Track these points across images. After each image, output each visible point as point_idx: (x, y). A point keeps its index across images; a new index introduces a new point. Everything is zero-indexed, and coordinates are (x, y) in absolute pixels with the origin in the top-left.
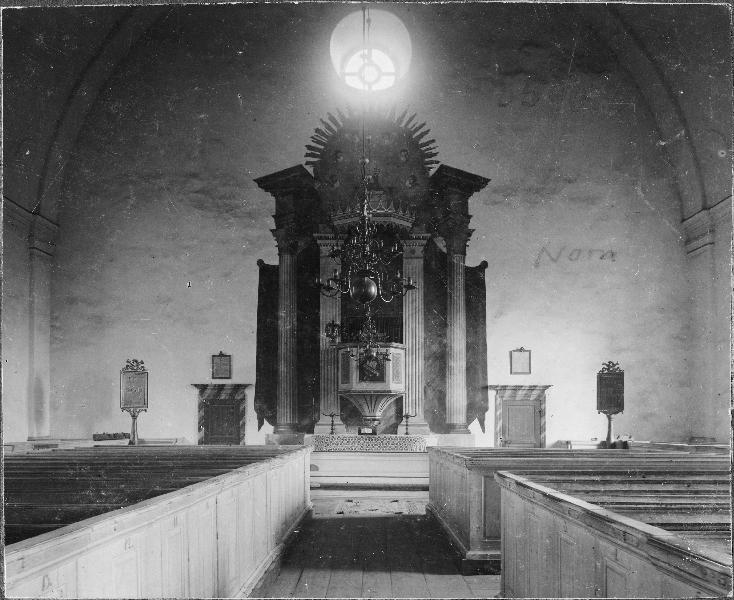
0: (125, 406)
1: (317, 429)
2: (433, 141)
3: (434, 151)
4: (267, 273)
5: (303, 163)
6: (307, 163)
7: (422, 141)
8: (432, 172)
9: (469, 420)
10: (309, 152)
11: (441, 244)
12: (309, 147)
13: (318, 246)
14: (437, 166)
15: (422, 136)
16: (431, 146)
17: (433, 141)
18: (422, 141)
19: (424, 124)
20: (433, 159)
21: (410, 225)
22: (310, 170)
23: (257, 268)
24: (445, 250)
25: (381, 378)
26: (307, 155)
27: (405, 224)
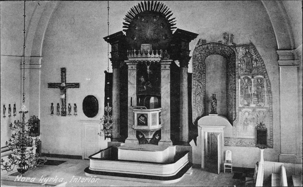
0: (40, 141)
1: (126, 141)
2: (174, 19)
3: (174, 23)
4: (108, 76)
5: (122, 30)
6: (124, 30)
7: (170, 19)
8: (173, 32)
9: (190, 140)
10: (124, 25)
11: (177, 63)
12: (124, 23)
13: (127, 66)
14: (176, 29)
15: (169, 17)
16: (173, 20)
17: (174, 19)
18: (170, 19)
19: (52, 104)
20: (174, 26)
21: (159, 59)
22: (125, 33)
23: (105, 74)
24: (179, 66)
25: (146, 124)
26: (123, 27)
27: (156, 59)
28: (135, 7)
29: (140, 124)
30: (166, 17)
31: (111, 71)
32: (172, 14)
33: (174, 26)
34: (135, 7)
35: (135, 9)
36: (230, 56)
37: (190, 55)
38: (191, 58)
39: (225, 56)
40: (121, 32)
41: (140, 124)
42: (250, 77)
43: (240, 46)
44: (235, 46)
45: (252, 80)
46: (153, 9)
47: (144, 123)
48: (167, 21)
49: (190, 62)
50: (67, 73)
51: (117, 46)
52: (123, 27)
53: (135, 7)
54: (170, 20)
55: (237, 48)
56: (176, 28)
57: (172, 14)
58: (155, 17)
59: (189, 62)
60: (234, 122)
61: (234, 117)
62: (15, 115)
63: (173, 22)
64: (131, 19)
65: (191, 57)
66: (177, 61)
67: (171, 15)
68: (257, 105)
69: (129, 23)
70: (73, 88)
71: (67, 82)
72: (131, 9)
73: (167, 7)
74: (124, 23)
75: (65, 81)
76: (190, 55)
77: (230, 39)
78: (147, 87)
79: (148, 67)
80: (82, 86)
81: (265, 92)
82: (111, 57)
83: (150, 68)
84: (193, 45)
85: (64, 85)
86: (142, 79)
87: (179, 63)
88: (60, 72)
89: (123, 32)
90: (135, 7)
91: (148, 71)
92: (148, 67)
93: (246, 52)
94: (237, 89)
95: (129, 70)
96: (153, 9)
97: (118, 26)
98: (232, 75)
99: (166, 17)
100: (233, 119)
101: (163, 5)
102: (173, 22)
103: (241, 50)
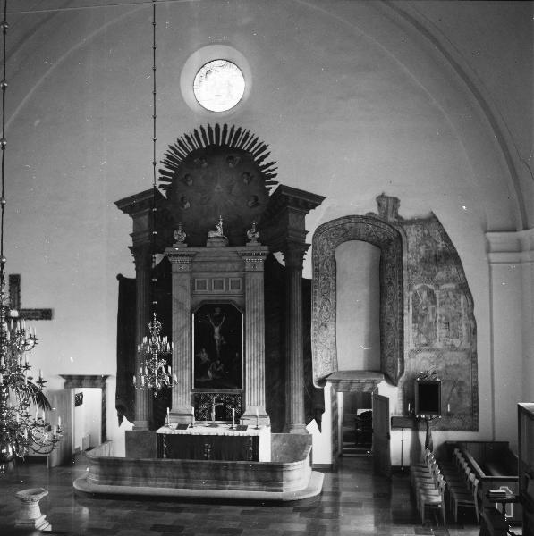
2: (272, 163)
3: (272, 173)
6: (161, 186)
7: (264, 163)
10: (162, 176)
11: (280, 257)
12: (162, 172)
14: (276, 187)
16: (271, 167)
18: (264, 163)
20: (273, 179)
22: (164, 193)
23: (118, 282)
24: (283, 264)
26: (161, 179)
30: (256, 159)
31: (131, 273)
32: (268, 154)
33: (273, 179)
35: (186, 141)
36: (389, 244)
39: (377, 244)
40: (155, 190)
42: (431, 286)
43: (412, 222)
44: (402, 222)
45: (437, 293)
46: (226, 143)
49: (308, 257)
51: (145, 220)
55: (405, 227)
57: (268, 154)
58: (232, 158)
59: (305, 257)
63: (270, 170)
64: (177, 162)
70: (37, 319)
71: (23, 307)
72: (179, 141)
73: (275, 175)
74: (162, 172)
78: (213, 372)
79: (217, 330)
80: (56, 315)
81: (463, 318)
83: (220, 332)
86: (204, 356)
89: (161, 190)
91: (217, 337)
92: (217, 330)
93: (424, 235)
94: (405, 311)
95: (177, 272)
96: (226, 143)
97: (145, 178)
98: (394, 283)
99: (256, 159)
100: (398, 374)
102: (270, 170)
103: (414, 232)
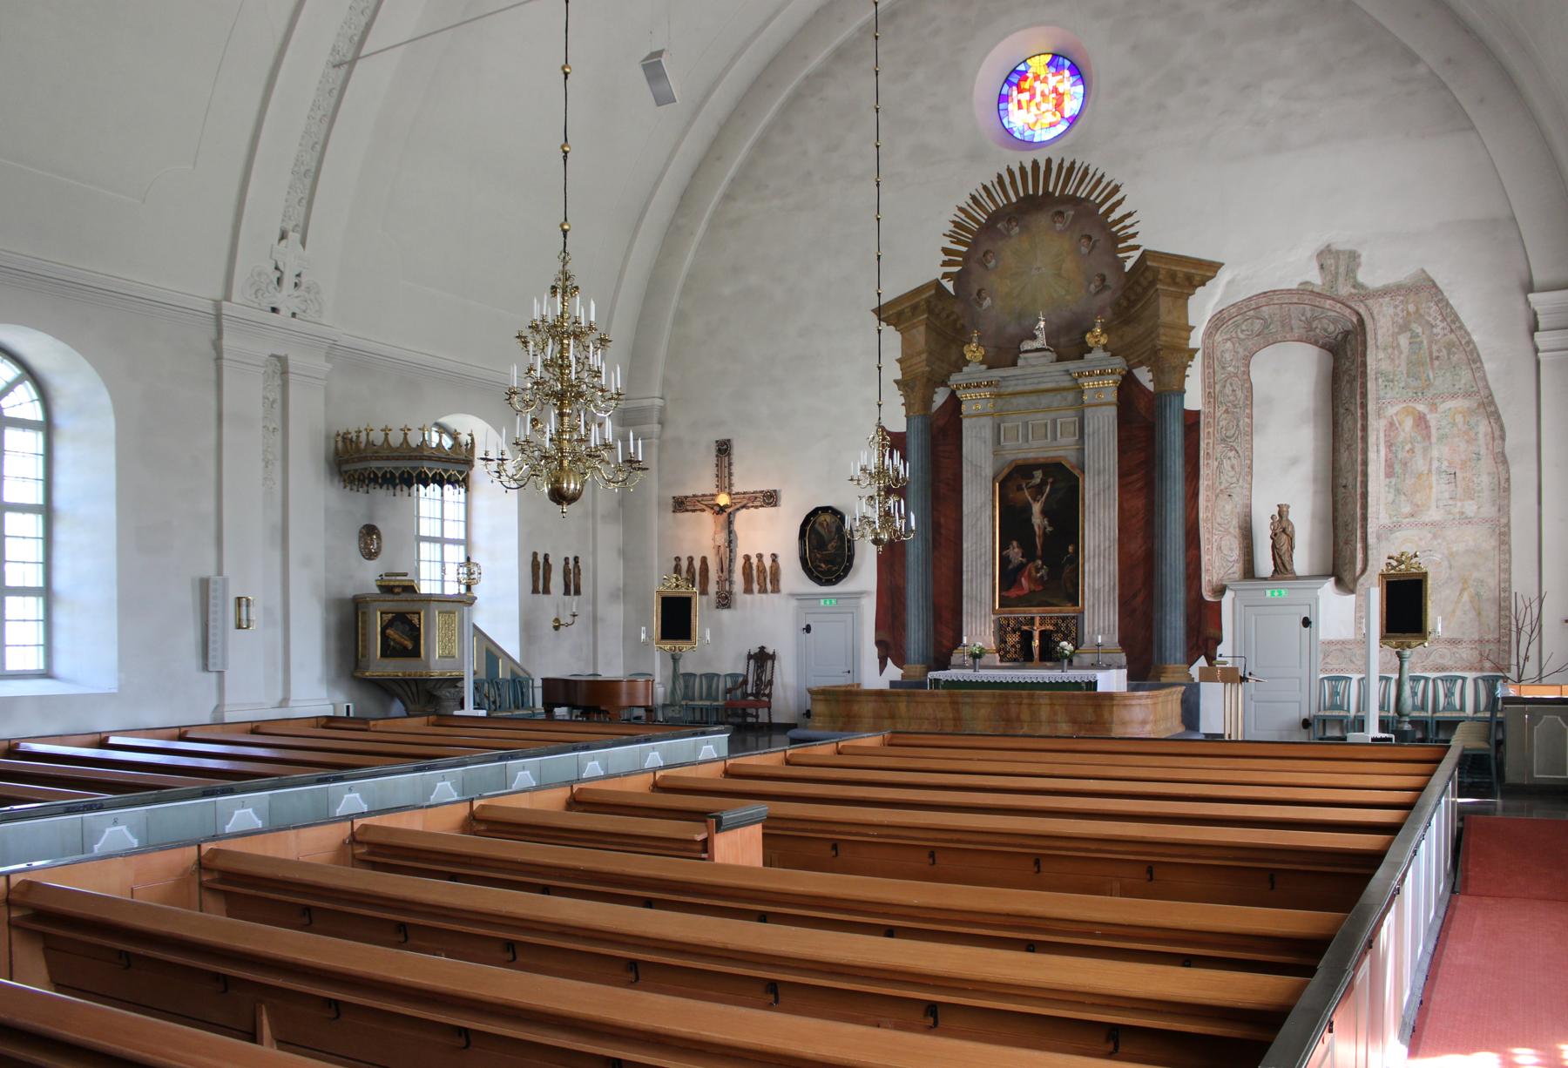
2: (1130, 215)
3: (1131, 231)
6: (945, 276)
8: (1129, 265)
12: (946, 251)
14: (1136, 254)
16: (1128, 222)
17: (1130, 215)
20: (1131, 242)
22: (949, 285)
26: (945, 264)
28: (985, 188)
29: (389, 651)
30: (1101, 210)
33: (1131, 242)
34: (961, 209)
37: (1192, 344)
38: (1199, 356)
40: (937, 285)
41: (389, 651)
44: (1365, 294)
45: (1432, 419)
47: (405, 648)
48: (1104, 224)
50: (735, 458)
51: (920, 334)
52: (945, 264)
53: (985, 188)
54: (1116, 222)
56: (1137, 247)
60: (1361, 580)
61: (1359, 566)
62: (572, 499)
65: (1196, 350)
66: (1144, 369)
67: (1119, 203)
68: (1449, 513)
69: (964, 249)
74: (946, 251)
75: (730, 485)
76: (1192, 344)
77: (1342, 270)
82: (899, 377)
84: (1203, 307)
85: (723, 500)
87: (1150, 376)
88: (714, 453)
90: (961, 209)
101: (1087, 169)
